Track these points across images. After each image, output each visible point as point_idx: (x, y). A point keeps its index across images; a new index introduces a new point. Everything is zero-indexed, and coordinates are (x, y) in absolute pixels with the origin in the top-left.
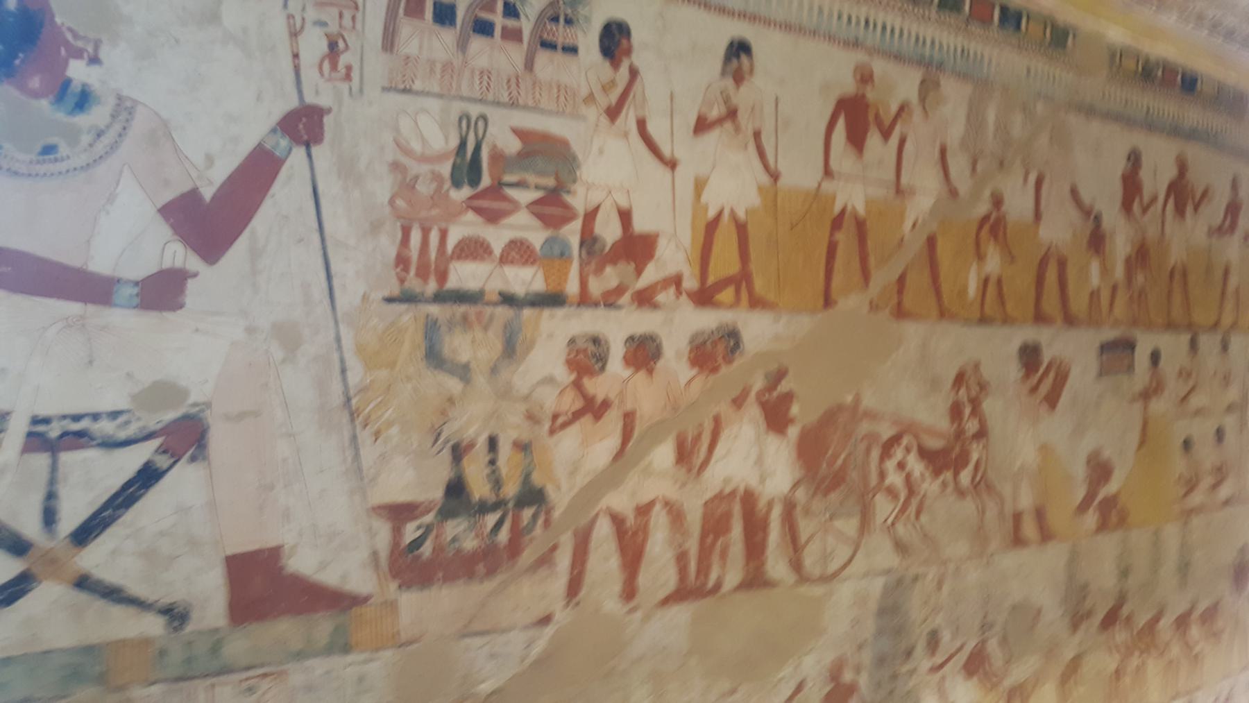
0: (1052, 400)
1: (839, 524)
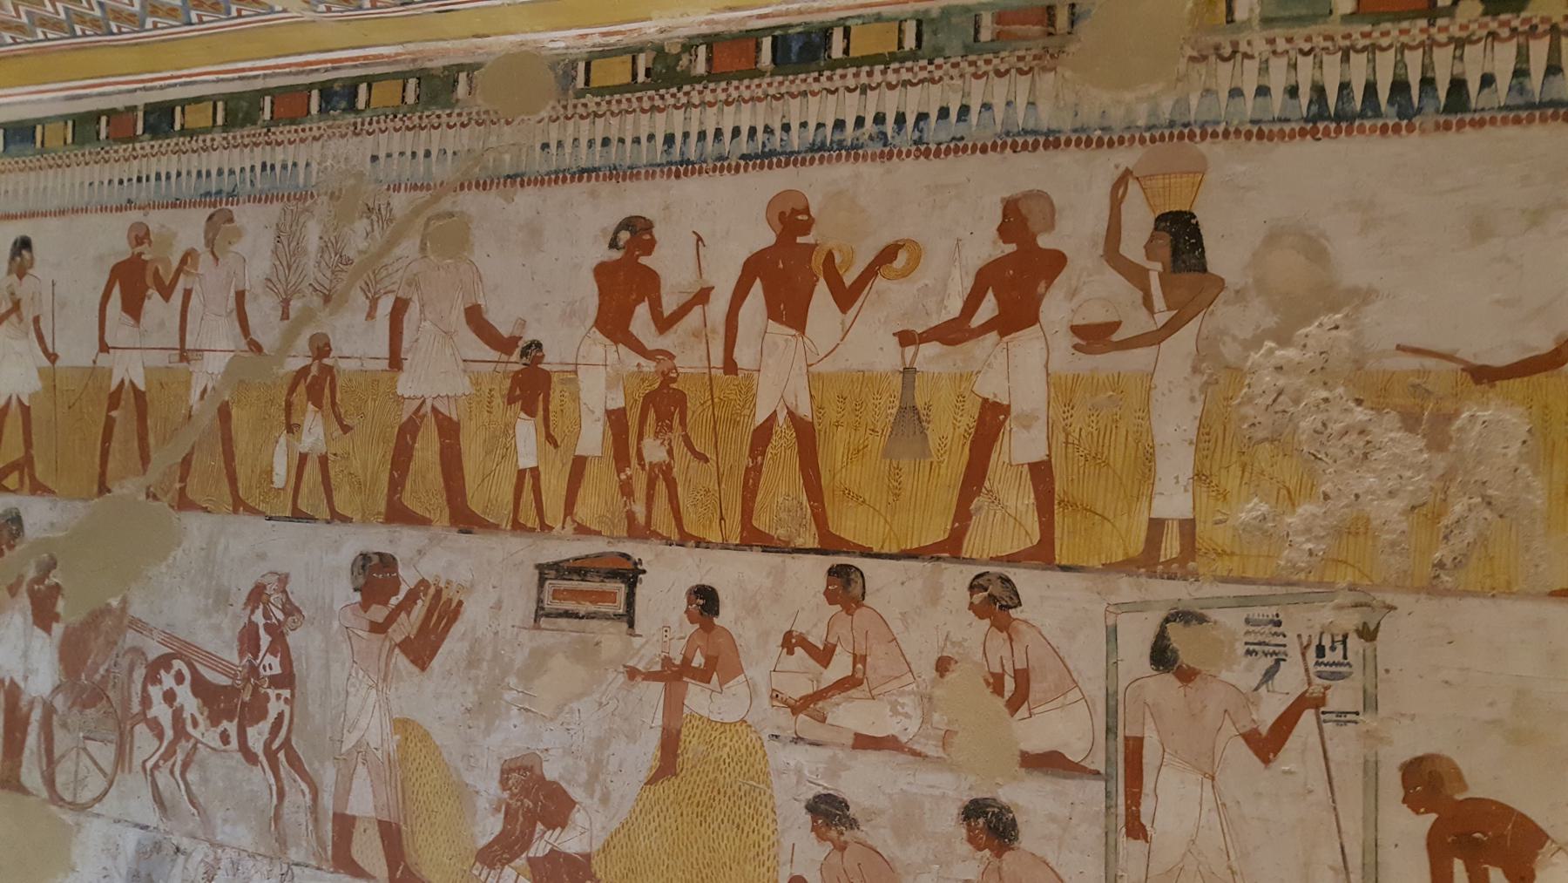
0: (421, 650)
1: (92, 746)
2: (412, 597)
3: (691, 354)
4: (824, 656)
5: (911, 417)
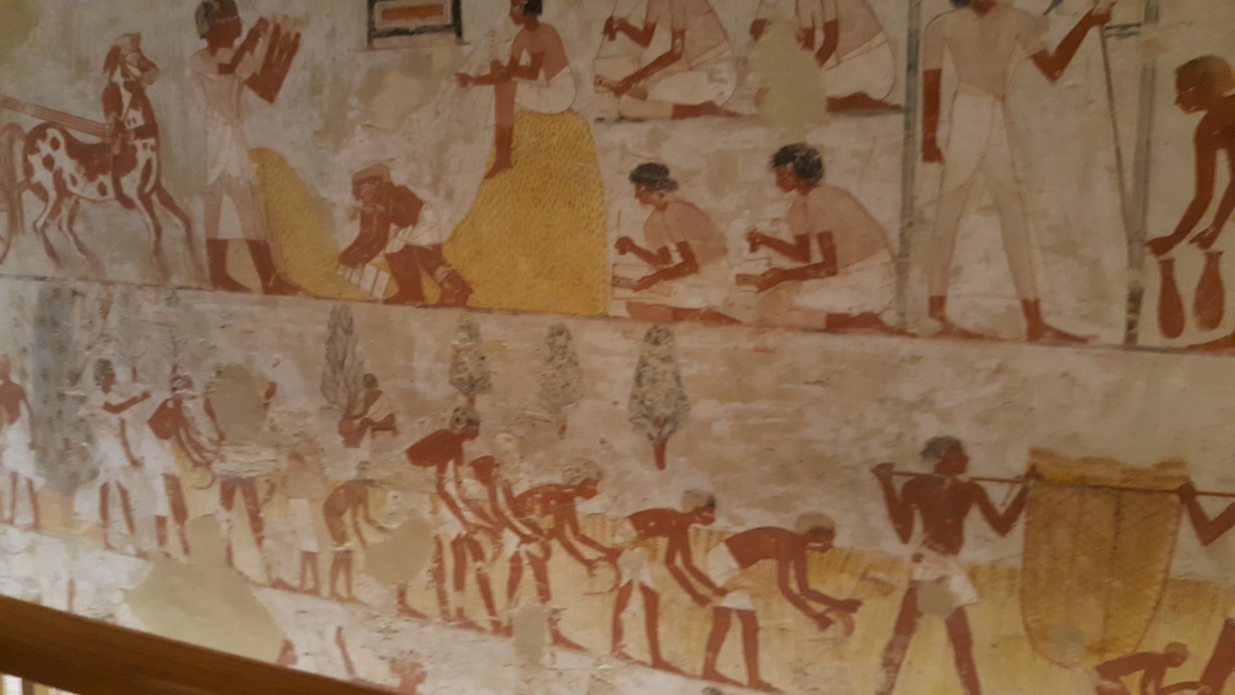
0: (267, 84)
2: (254, 35)
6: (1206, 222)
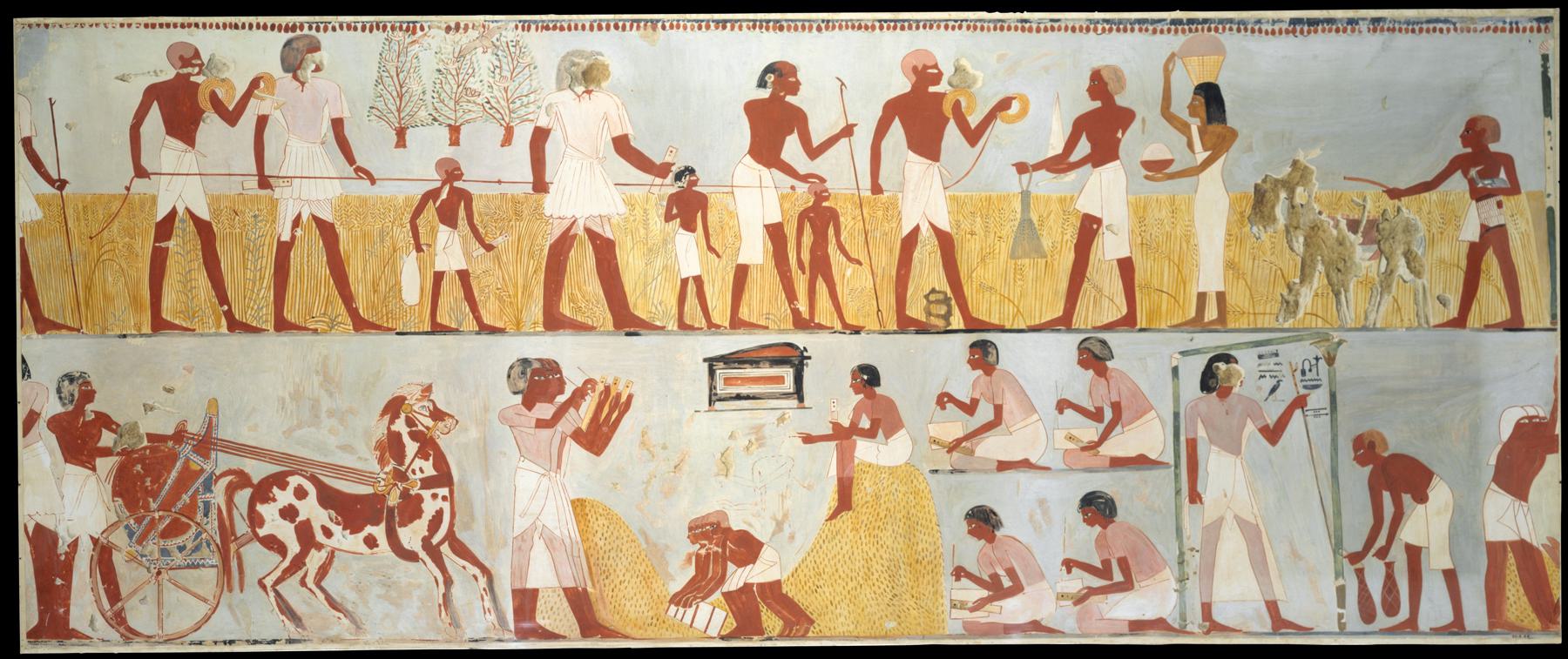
0: (595, 438)
2: (579, 395)
3: (841, 171)
4: (970, 408)
5: (1028, 231)
6: (1381, 541)
